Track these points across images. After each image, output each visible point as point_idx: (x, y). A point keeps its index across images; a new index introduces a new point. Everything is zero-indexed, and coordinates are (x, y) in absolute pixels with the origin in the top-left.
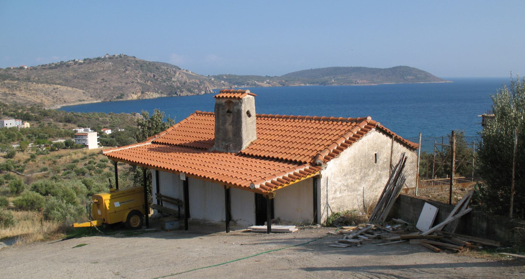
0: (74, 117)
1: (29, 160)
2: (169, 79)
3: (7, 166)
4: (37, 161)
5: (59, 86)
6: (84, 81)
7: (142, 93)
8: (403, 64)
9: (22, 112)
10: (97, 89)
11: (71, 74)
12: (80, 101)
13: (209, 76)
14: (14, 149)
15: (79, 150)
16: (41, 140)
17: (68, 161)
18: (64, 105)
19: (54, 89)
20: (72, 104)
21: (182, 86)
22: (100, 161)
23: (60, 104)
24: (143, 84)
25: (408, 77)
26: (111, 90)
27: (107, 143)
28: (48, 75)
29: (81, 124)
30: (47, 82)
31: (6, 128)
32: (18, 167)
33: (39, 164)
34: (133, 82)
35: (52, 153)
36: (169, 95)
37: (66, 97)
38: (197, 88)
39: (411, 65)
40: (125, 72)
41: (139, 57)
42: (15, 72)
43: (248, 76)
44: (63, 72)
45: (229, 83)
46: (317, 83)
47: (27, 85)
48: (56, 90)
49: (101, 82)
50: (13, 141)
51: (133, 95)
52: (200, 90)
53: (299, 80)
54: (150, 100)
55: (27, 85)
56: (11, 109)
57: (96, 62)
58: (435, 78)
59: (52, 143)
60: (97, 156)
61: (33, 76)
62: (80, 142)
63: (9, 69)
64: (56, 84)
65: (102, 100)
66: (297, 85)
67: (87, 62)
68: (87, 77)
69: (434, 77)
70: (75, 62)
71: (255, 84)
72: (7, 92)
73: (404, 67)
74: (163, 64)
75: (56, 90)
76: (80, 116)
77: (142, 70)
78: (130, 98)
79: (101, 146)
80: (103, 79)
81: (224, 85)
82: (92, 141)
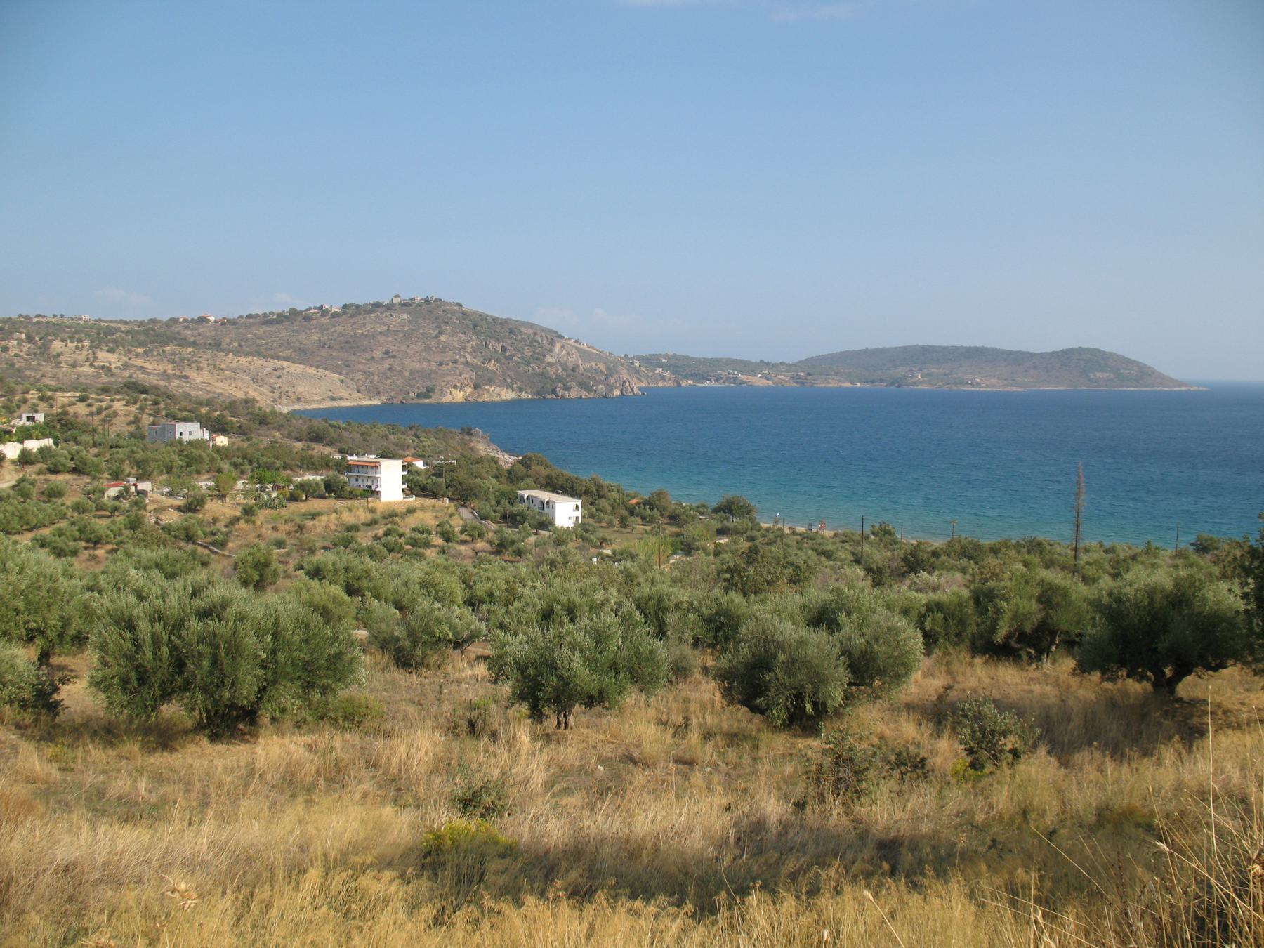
0: (331, 430)
1: (238, 519)
2: (539, 358)
3: (187, 529)
4: (258, 523)
5: (286, 364)
6: (342, 354)
7: (476, 387)
8: (1075, 344)
9: (208, 413)
10: (372, 374)
11: (315, 338)
12: (333, 399)
13: (626, 356)
14: (203, 491)
15: (357, 502)
16: (268, 474)
17: (333, 527)
18: (297, 407)
19: (275, 370)
20: (314, 406)
21: (568, 376)
22: (413, 530)
23: (288, 404)
24: (479, 367)
25: (1099, 375)
26: (404, 377)
27: (423, 489)
28: (261, 338)
29: (345, 446)
30: (259, 354)
31: (180, 442)
32: (214, 534)
33: (264, 530)
34: (455, 362)
35: (293, 507)
36: (538, 394)
37: (301, 389)
38: (601, 382)
39: (1107, 347)
40: (437, 337)
41: (470, 305)
42: (187, 328)
43: (718, 360)
44: (296, 332)
45: (675, 373)
46: (881, 381)
47: (213, 358)
48: (279, 373)
49: (382, 359)
50: (198, 472)
51: (454, 391)
52: (610, 388)
53: (837, 373)
54: (493, 404)
55: (213, 358)
56: (184, 404)
57: (371, 311)
58: (1163, 379)
59: (291, 482)
60: (403, 519)
61: (227, 340)
62: (360, 482)
63: (174, 321)
64: (279, 358)
65: (384, 399)
66: (833, 384)
67: (350, 311)
68: (352, 344)
69: (1160, 376)
70: (324, 312)
71: (735, 380)
72: (170, 372)
73: (1088, 349)
74: (524, 324)
75: (279, 373)
76: (345, 429)
77: (478, 334)
78: (447, 399)
79: (407, 495)
80: (387, 352)
81: (663, 378)
82: (390, 481)
